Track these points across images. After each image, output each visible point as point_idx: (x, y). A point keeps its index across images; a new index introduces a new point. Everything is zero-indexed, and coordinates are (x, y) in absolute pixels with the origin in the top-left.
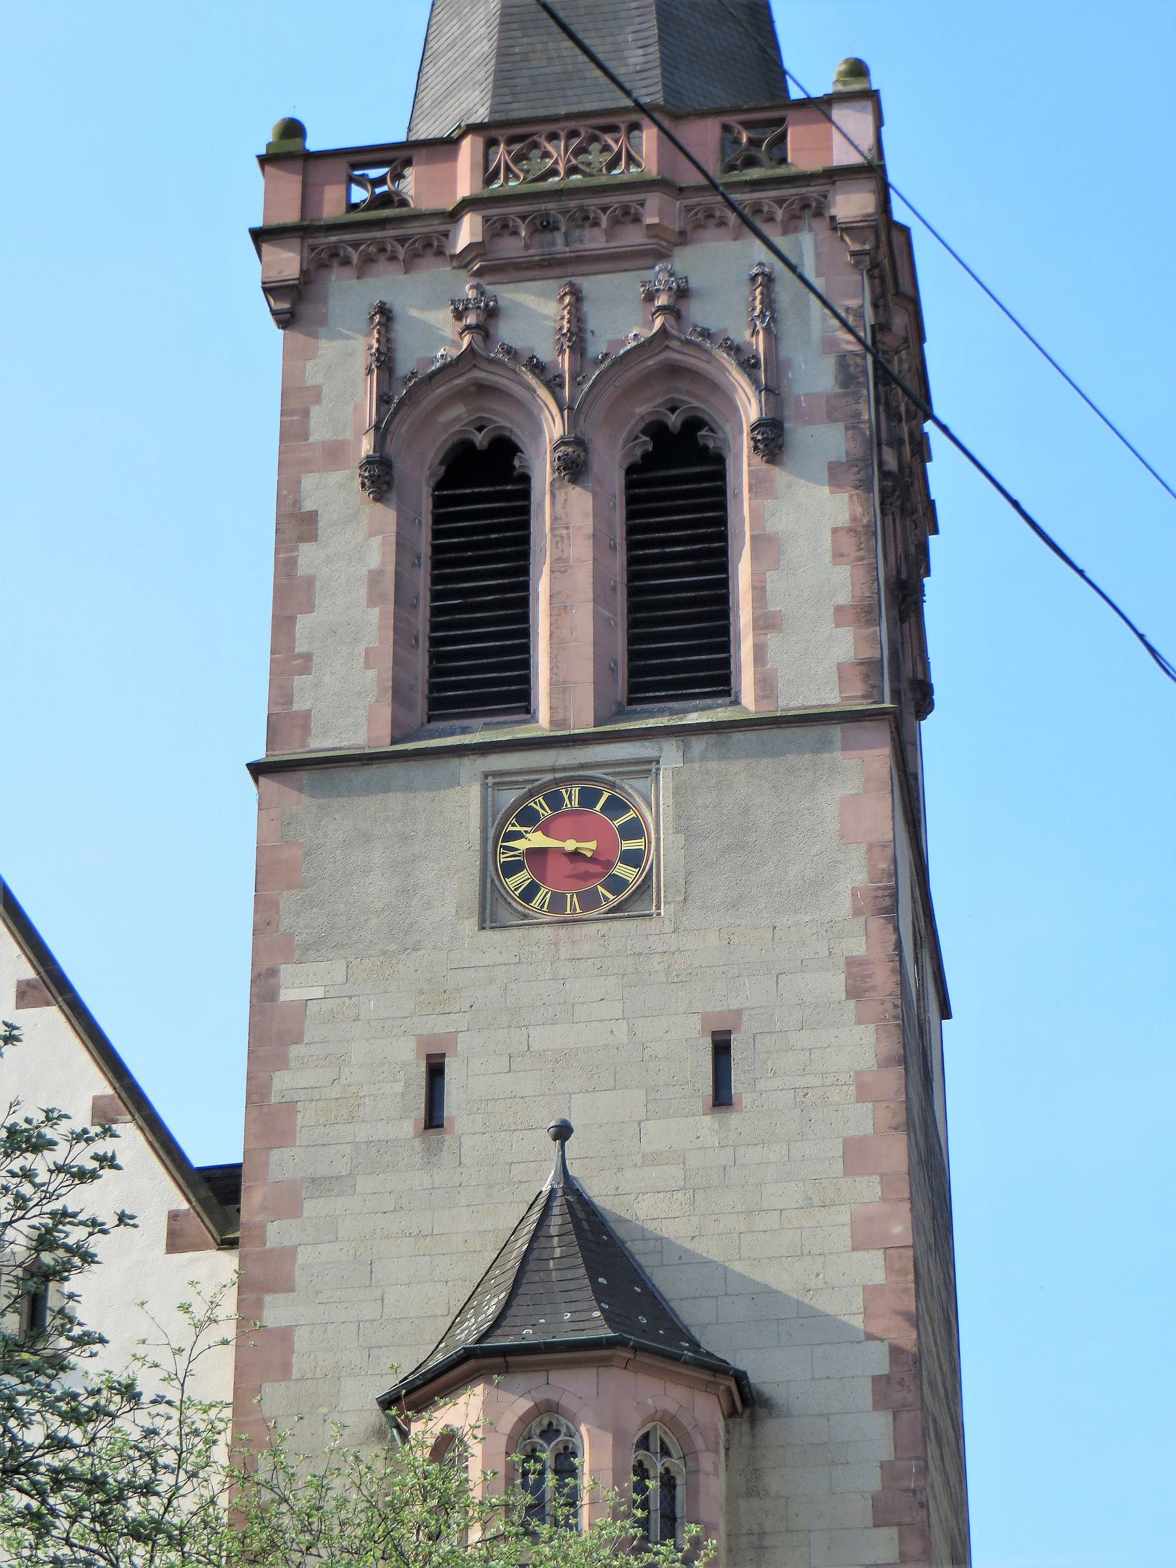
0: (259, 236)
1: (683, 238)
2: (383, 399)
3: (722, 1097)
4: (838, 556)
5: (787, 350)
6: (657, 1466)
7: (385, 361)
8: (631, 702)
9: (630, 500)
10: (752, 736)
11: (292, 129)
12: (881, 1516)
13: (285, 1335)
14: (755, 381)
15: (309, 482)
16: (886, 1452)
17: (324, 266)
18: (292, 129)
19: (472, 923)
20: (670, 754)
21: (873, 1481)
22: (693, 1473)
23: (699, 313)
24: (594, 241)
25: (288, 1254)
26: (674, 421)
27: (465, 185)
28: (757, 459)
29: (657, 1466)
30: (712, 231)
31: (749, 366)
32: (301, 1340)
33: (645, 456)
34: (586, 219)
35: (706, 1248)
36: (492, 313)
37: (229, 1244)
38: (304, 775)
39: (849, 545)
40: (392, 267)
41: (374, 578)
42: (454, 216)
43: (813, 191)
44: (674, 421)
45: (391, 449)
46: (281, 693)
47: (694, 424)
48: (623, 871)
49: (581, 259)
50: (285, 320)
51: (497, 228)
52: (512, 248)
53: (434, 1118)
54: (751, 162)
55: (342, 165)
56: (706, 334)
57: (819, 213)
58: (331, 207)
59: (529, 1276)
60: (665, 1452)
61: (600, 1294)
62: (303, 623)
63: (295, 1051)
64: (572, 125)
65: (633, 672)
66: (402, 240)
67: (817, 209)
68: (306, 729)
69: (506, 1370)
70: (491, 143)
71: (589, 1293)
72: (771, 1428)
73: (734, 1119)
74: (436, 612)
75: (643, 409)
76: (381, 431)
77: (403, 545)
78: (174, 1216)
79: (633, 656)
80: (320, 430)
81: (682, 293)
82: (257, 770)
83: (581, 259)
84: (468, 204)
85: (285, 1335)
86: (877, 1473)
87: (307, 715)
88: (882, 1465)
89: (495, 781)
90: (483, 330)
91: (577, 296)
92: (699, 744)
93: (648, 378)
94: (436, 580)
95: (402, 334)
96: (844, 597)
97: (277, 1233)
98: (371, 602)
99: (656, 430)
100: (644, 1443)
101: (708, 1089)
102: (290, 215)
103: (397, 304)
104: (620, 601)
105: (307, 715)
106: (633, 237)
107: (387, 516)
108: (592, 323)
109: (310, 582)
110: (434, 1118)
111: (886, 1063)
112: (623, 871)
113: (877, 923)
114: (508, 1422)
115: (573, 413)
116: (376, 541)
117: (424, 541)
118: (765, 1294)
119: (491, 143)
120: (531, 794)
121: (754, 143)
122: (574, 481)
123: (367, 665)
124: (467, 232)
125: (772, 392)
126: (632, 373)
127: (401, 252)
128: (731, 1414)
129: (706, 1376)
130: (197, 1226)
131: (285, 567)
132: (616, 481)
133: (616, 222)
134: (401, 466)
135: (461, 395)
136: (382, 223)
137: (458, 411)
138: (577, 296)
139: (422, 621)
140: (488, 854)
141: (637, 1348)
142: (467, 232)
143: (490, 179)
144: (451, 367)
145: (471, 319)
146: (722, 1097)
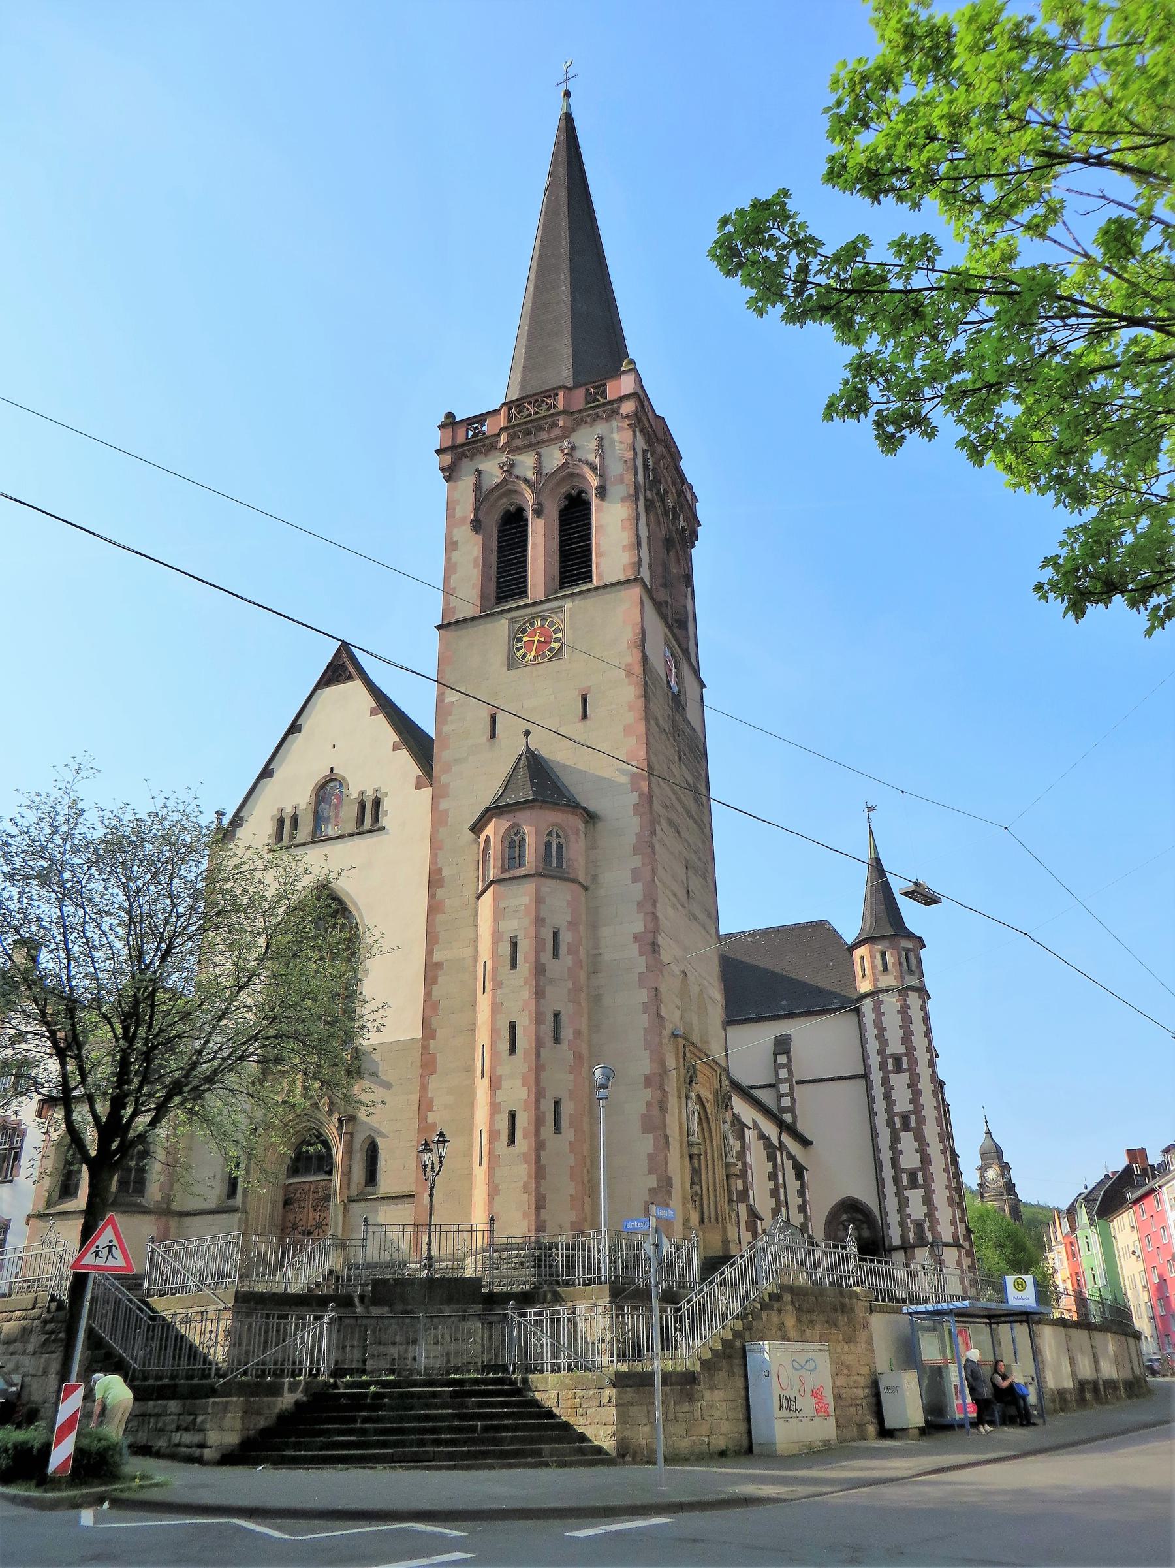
0: (438, 452)
1: (573, 430)
2: (477, 500)
3: (585, 716)
4: (624, 528)
5: (607, 462)
6: (555, 842)
7: (478, 487)
8: (560, 588)
9: (561, 521)
10: (593, 593)
11: (450, 415)
12: (636, 850)
13: (446, 812)
14: (596, 474)
15: (455, 531)
16: (638, 829)
17: (460, 459)
18: (450, 415)
19: (506, 668)
20: (569, 604)
21: (633, 840)
22: (568, 843)
23: (578, 454)
24: (544, 435)
25: (447, 785)
26: (574, 492)
27: (503, 423)
28: (597, 500)
29: (555, 842)
30: (584, 426)
31: (593, 468)
32: (451, 814)
33: (566, 506)
34: (541, 429)
35: (581, 767)
36: (512, 465)
37: (431, 785)
38: (453, 627)
39: (627, 524)
40: (587, 425)
41: (475, 560)
42: (499, 435)
43: (615, 406)
44: (574, 492)
45: (481, 516)
46: (446, 603)
47: (581, 492)
48: (554, 645)
49: (539, 443)
50: (448, 479)
51: (512, 437)
52: (518, 442)
53: (493, 735)
54: (596, 400)
55: (465, 424)
56: (580, 461)
57: (618, 413)
58: (461, 439)
59: (511, 782)
60: (558, 836)
61: (533, 785)
62: (453, 578)
63: (450, 718)
64: (535, 397)
65: (561, 578)
66: (483, 446)
67: (616, 412)
68: (454, 612)
69: (502, 814)
70: (510, 409)
71: (529, 786)
72: (600, 825)
73: (588, 722)
74: (498, 568)
75: (563, 490)
76: (476, 510)
77: (485, 547)
78: (417, 777)
79: (561, 573)
80: (459, 513)
81: (573, 448)
82: (438, 627)
83: (539, 443)
84: (503, 429)
85: (446, 812)
86: (634, 837)
87: (454, 608)
88: (636, 834)
89: (513, 621)
90: (509, 472)
91: (539, 455)
92: (578, 598)
93: (563, 479)
94: (499, 558)
95: (484, 477)
96: (626, 542)
97: (444, 779)
98: (474, 567)
99: (569, 497)
100: (550, 834)
101: (580, 714)
102: (449, 444)
103: (481, 467)
104: (556, 556)
105: (454, 608)
106: (556, 432)
107: (479, 539)
108: (544, 464)
109: (456, 564)
110: (493, 735)
111: (638, 697)
112: (554, 645)
113: (635, 650)
114: (502, 831)
115: (537, 494)
116: (476, 547)
117: (494, 545)
118: (600, 779)
119: (510, 409)
120: (525, 623)
121: (596, 393)
122: (538, 517)
123: (473, 588)
124: (503, 439)
125: (601, 476)
126: (557, 478)
127: (589, 420)
128: (586, 822)
129: (571, 809)
130: (425, 780)
131: (448, 560)
132: (555, 515)
133: (550, 428)
134: (485, 521)
135: (504, 494)
136: (477, 441)
137: (505, 500)
138: (539, 455)
139: (494, 571)
140: (510, 646)
141: (543, 801)
142: (503, 439)
143: (510, 420)
144: (498, 485)
145: (505, 468)
146: (585, 716)
